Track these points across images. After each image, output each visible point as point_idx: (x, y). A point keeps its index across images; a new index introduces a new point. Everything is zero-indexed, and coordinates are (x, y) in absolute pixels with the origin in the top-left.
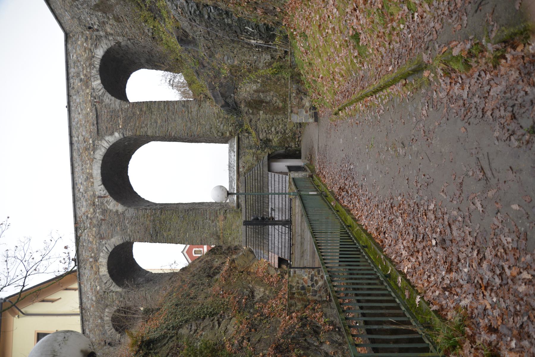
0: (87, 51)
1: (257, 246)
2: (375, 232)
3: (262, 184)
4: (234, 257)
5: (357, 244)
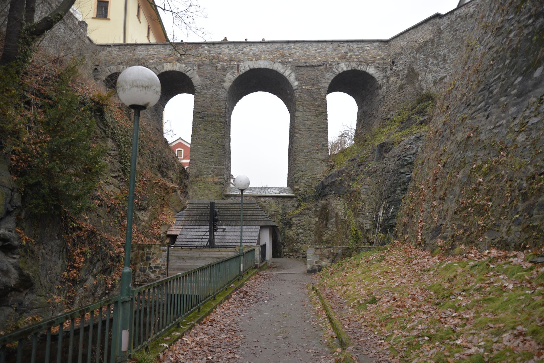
0: (372, 59)
1: (188, 214)
2: (211, 319)
3: (249, 219)
4: (179, 192)
5: (201, 303)
